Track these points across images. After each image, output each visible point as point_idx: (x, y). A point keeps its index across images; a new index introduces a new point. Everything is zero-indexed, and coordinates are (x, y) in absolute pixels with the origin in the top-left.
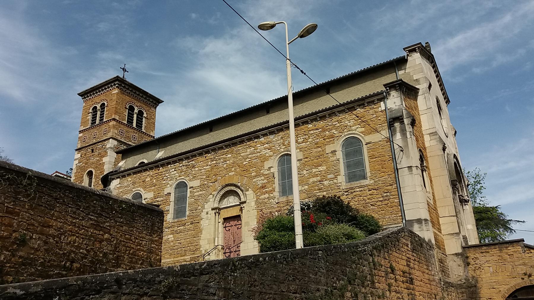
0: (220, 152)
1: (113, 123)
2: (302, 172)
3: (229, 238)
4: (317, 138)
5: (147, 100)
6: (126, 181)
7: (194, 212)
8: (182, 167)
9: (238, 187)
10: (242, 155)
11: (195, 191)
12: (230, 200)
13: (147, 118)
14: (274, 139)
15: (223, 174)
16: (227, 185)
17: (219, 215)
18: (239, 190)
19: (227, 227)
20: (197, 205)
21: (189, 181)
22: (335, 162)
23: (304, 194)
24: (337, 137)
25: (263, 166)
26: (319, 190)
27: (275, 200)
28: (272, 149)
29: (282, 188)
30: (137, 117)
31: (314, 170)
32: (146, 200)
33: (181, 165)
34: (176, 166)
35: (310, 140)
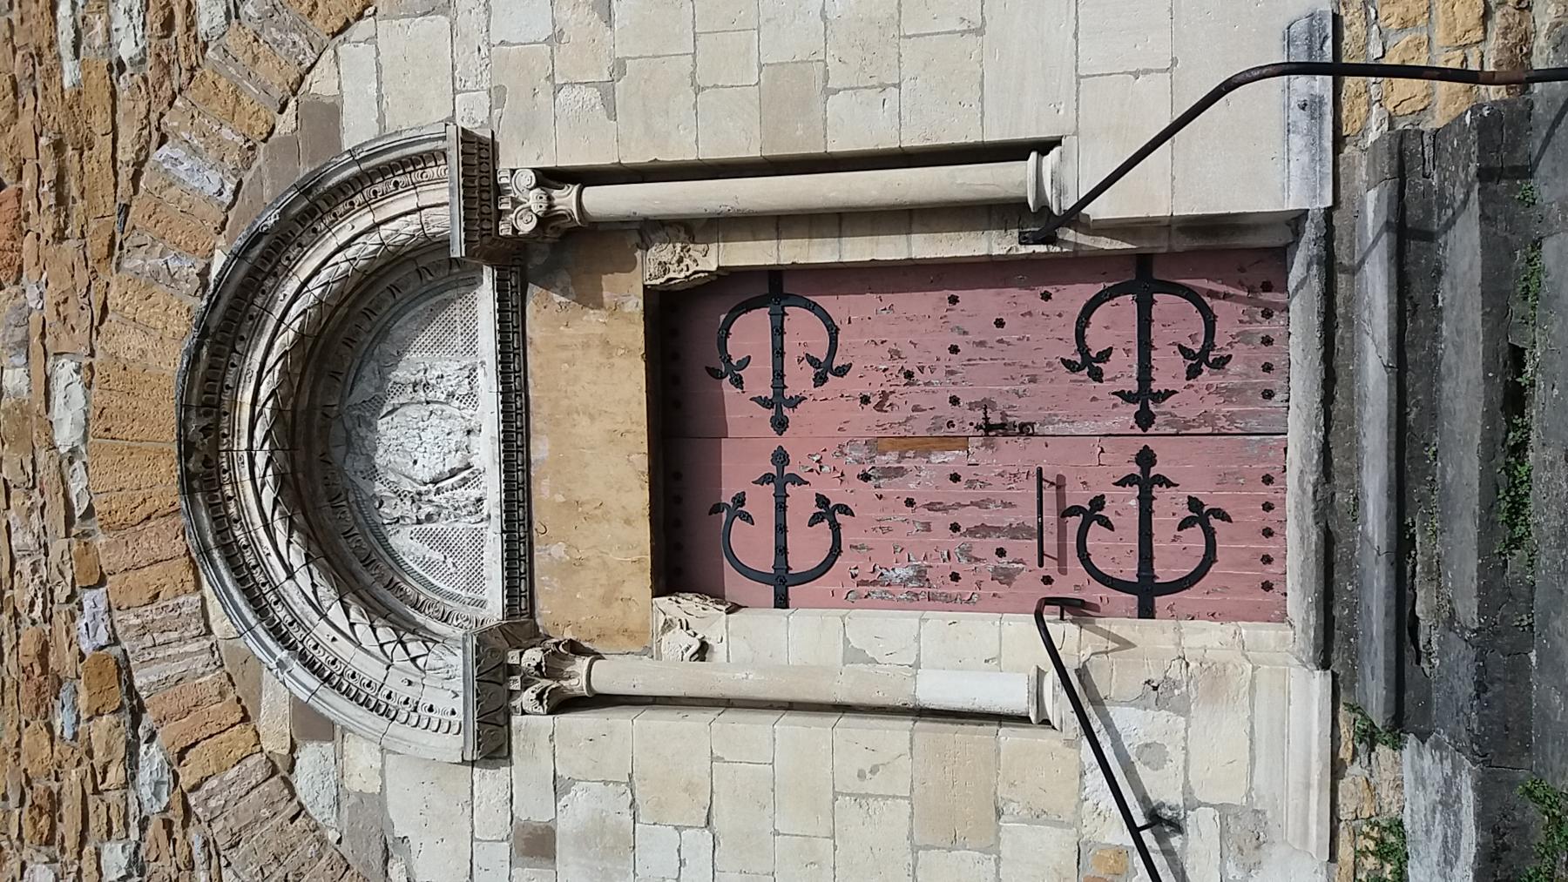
3: (941, 521)
19: (782, 550)
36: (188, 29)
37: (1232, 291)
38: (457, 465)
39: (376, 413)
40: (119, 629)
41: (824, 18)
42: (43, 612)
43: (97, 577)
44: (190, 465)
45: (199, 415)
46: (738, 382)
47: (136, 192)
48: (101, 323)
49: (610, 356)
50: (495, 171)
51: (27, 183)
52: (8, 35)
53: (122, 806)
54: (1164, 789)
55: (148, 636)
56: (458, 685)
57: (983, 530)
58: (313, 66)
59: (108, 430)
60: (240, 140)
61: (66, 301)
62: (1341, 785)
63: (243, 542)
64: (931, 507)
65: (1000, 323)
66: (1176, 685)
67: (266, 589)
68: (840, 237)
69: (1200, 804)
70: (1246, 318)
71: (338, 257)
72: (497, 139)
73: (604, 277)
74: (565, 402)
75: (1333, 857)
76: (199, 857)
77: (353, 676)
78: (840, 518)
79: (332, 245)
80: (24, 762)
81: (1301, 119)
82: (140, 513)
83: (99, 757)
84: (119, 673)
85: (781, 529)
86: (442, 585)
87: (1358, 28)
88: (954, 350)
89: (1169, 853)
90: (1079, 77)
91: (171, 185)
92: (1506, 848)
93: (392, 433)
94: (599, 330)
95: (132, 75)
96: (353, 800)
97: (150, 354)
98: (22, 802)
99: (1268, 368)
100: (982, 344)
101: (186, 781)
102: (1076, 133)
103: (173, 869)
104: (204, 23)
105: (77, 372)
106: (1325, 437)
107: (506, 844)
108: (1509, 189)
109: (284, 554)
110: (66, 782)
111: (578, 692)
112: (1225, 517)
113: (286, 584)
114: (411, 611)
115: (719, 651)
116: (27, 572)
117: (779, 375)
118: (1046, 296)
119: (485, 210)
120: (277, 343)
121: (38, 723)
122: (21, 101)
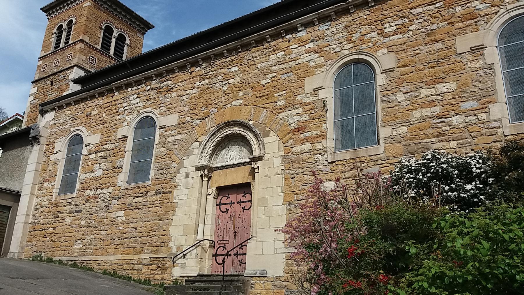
0: (218, 63)
1: (80, 46)
2: (392, 98)
4: (432, 21)
5: (132, 21)
6: (64, 115)
7: (164, 171)
8: (150, 90)
9: (248, 128)
10: (259, 66)
11: (168, 133)
13: (131, 46)
14: (328, 32)
15: (222, 104)
16: (227, 124)
17: (208, 181)
18: (251, 135)
19: (223, 204)
20: (170, 159)
21: (159, 116)
22: (481, 71)
23: (398, 145)
24: (486, 15)
25: (302, 87)
26: (438, 136)
27: (325, 156)
28: (322, 51)
29: (342, 132)
30: (116, 43)
31: (424, 92)
32: (88, 147)
33: (148, 87)
34: (140, 90)
35: (414, 27)
54: (188, 256)
73: (252, 176)
75: (180, 277)
78: (226, 212)
80: (199, 104)
83: (199, 115)
87: (264, 280)
88: (245, 227)
114: (215, 154)
121: (203, 105)
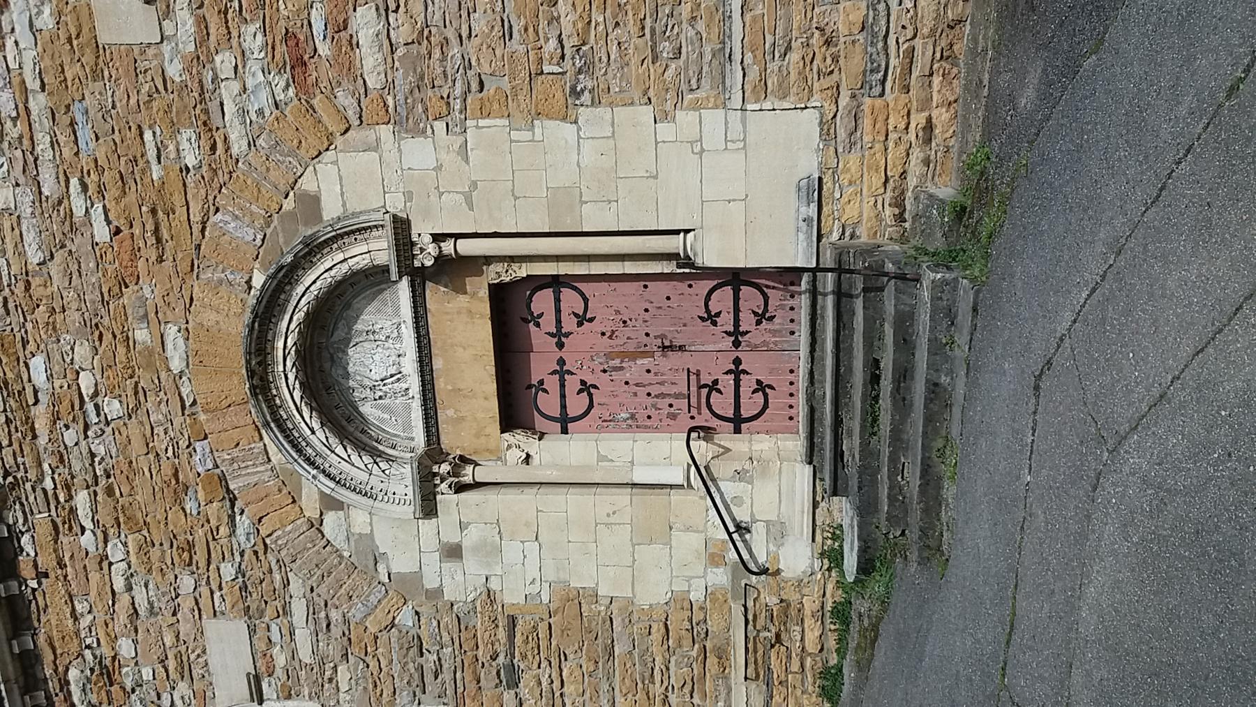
3: (642, 391)
10: (34, 257)
11: (281, 660)
12: (377, 373)
15: (178, 420)
16: (261, 384)
19: (564, 407)
25: (134, 57)
36: (226, 151)
37: (776, 285)
38: (394, 372)
39: (347, 346)
40: (219, 462)
41: (579, 166)
42: (174, 453)
43: (203, 436)
44: (254, 382)
45: (256, 356)
46: (538, 325)
47: (203, 237)
48: (191, 306)
49: (472, 318)
50: (410, 234)
51: (137, 231)
52: (114, 148)
53: (229, 545)
54: (742, 515)
55: (235, 464)
56: (409, 481)
57: (662, 396)
58: (302, 175)
59: (201, 362)
60: (263, 212)
61: (168, 294)
62: (817, 511)
63: (285, 417)
64: (637, 385)
65: (668, 298)
66: (747, 471)
67: (300, 440)
68: (589, 261)
69: (758, 521)
70: (782, 298)
71: (326, 275)
72: (410, 218)
74: (449, 341)
75: (813, 540)
76: (275, 567)
77: (352, 480)
78: (592, 390)
79: (322, 269)
80: (171, 527)
81: (803, 225)
82: (225, 403)
83: (213, 523)
84: (221, 482)
85: (563, 396)
86: (390, 430)
88: (646, 310)
89: (745, 541)
90: (703, 201)
91: (224, 234)
92: (869, 547)
93: (357, 356)
94: (466, 305)
95: (195, 175)
96: (356, 537)
97: (222, 323)
98: (172, 546)
99: (792, 321)
100: (660, 308)
101: (263, 533)
102: (702, 228)
103: (261, 574)
104: (236, 149)
105: (179, 331)
106: (811, 367)
107: (438, 553)
108: (874, 296)
109: (308, 422)
110: (196, 536)
111: (468, 482)
112: (772, 388)
113: (311, 437)
114: (376, 444)
115: (536, 460)
116: (162, 434)
117: (559, 321)
118: (690, 286)
119: (406, 255)
120: (295, 318)
121: (177, 507)
122: (127, 186)
